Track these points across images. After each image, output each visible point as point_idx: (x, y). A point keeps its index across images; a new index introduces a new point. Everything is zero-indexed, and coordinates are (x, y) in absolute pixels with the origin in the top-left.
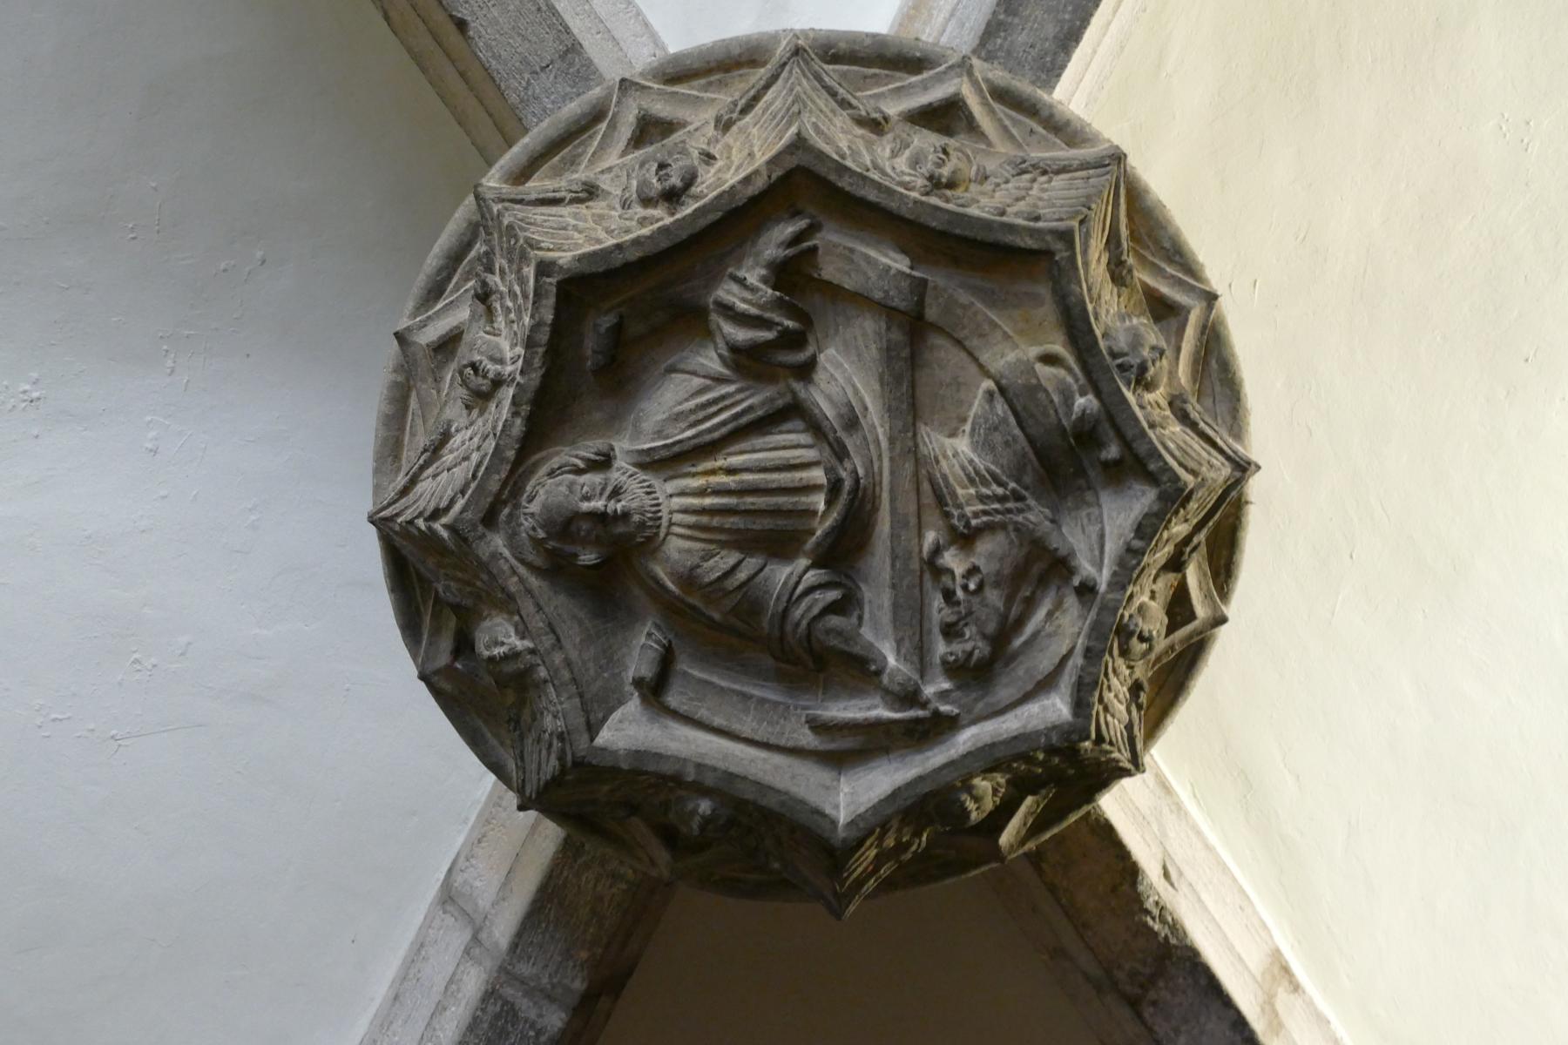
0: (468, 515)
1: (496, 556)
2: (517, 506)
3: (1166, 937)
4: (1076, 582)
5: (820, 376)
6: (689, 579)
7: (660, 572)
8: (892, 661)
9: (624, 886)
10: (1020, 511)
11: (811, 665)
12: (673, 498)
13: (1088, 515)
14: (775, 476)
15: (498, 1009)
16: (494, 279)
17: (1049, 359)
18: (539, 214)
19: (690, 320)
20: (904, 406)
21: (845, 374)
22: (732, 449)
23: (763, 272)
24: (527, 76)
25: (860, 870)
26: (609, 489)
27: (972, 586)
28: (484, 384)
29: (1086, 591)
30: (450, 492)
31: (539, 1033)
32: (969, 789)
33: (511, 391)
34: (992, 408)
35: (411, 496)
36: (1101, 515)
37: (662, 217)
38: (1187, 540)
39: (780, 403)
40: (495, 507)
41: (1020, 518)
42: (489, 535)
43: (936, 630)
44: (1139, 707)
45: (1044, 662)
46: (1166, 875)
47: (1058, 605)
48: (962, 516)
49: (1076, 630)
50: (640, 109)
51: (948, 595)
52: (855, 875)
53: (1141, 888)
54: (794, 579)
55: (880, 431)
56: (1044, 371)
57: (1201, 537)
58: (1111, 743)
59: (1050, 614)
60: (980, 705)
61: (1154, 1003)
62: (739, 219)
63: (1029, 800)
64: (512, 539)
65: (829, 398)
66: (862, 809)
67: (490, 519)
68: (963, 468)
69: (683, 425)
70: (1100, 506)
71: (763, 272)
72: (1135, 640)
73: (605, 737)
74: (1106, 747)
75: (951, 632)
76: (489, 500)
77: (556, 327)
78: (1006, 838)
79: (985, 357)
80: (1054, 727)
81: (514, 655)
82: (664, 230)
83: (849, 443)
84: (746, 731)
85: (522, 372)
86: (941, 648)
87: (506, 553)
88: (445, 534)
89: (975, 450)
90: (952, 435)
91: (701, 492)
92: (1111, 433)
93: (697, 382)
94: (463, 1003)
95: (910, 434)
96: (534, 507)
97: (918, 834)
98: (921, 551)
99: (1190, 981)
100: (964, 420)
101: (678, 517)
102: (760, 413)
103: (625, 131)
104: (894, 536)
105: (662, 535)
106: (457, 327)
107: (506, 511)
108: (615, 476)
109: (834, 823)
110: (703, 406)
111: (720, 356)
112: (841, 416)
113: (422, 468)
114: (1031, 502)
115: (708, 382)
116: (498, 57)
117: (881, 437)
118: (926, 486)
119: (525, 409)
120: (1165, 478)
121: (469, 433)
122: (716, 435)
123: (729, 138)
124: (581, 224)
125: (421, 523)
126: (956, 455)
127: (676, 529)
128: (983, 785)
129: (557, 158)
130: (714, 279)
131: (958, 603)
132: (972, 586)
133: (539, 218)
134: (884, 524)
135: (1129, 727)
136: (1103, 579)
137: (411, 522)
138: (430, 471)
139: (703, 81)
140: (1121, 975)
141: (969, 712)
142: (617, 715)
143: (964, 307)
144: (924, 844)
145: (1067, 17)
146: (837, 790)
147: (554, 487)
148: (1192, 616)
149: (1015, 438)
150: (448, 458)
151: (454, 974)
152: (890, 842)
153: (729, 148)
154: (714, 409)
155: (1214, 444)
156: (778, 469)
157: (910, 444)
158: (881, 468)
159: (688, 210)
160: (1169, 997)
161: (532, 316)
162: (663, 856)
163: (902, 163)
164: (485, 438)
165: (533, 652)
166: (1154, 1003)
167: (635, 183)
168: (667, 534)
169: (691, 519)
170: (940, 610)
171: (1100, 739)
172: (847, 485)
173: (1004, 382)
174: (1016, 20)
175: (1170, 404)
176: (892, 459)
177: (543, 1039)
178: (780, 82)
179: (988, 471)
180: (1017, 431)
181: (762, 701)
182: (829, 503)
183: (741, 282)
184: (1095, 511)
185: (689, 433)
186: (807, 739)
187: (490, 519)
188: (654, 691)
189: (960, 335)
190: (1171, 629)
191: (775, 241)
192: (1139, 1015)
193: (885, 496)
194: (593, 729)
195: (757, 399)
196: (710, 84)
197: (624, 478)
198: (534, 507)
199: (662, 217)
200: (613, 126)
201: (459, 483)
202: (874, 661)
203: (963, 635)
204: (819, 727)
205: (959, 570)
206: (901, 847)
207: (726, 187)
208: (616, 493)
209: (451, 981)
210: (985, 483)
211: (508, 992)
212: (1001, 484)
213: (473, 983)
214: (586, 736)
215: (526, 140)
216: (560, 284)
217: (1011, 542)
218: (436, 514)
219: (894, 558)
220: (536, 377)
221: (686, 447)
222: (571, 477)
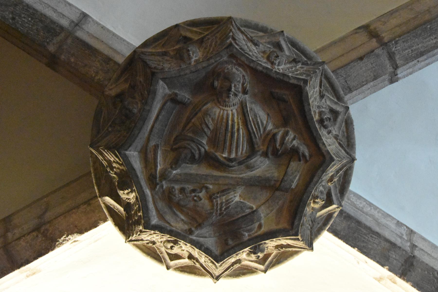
0: (235, 50)
1: (222, 57)
2: (235, 65)
3: (58, 241)
4: (193, 229)
5: (262, 159)
6: (206, 113)
7: (209, 105)
8: (174, 172)
9: (93, 75)
10: (216, 214)
11: (174, 147)
12: (232, 112)
13: (211, 234)
14: (235, 143)
15: (57, 31)
16: (300, 65)
17: (260, 226)
18: (318, 81)
19: (285, 121)
20: (251, 183)
21: (262, 167)
22: (244, 131)
23: (296, 146)
24: (345, 76)
25: (107, 155)
26: (237, 93)
27: (195, 198)
28: (273, 58)
29: (191, 232)
30: (241, 44)
31: (48, 43)
32: (132, 192)
33: (269, 67)
34: (248, 208)
35: (238, 32)
36: (211, 237)
37: (316, 118)
38: (197, 261)
39: (256, 146)
40: (237, 57)
41: (214, 214)
42: (227, 55)
43: (182, 186)
44: (148, 243)
45: (168, 217)
46: (75, 241)
47: (185, 223)
48: (217, 197)
49: (178, 228)
50: (341, 112)
51: (194, 191)
52: (107, 155)
53: (75, 234)
54: (203, 145)
55: (244, 175)
56: (257, 225)
57: (198, 265)
58: (139, 235)
59: (183, 220)
60: (157, 197)
61: (37, 236)
62: (314, 140)
63: (122, 209)
64: (226, 62)
65: (256, 161)
66: (129, 159)
67: (232, 56)
68: (231, 198)
69: (253, 117)
70: (214, 237)
71: (296, 146)
72: (172, 244)
73: (161, 82)
74: (139, 233)
75: (182, 190)
76: (239, 57)
77: (287, 83)
78: (108, 200)
79: (263, 207)
80: (149, 219)
81: (190, 58)
82: (312, 119)
83: (242, 166)
84: (156, 125)
85: (276, 71)
86: (177, 187)
87: (222, 60)
88: (228, 41)
89: (236, 202)
90: (240, 196)
91: (233, 121)
92: (236, 243)
93: (265, 122)
94: (57, 19)
95: (243, 184)
96: (234, 70)
97: (116, 173)
98: (207, 184)
99: (43, 248)
100: (244, 199)
101: (225, 112)
102: (254, 140)
103: (334, 107)
104: (213, 176)
105: (220, 107)
106: (284, 50)
107: (234, 61)
108: (240, 95)
109: (126, 150)
110: (258, 123)
111: (271, 130)
112: (251, 164)
113: (246, 36)
114: (219, 218)
115: (264, 125)
116: (351, 68)
117: (243, 175)
118: (226, 187)
119: (265, 71)
120: (222, 258)
121: (256, 52)
122: (249, 126)
123: (333, 138)
124: (315, 93)
125: (231, 34)
126: (235, 197)
127: (222, 112)
128: (132, 196)
129: (328, 86)
130: (294, 130)
131: (191, 193)
132: (195, 198)
133: (317, 80)
134: (216, 173)
135: (142, 240)
136: (194, 238)
137: (231, 30)
138: (245, 38)
139: (345, 130)
140: (47, 226)
141: (156, 194)
142: (166, 87)
143: (278, 203)
144: (112, 175)
145: (342, 233)
146: (135, 151)
147: (239, 74)
148: (171, 260)
149: (238, 215)
150: (249, 44)
151: (65, 16)
152: (114, 165)
153: (330, 139)
154: (257, 127)
155: (225, 271)
156: (237, 143)
157: (240, 183)
158: (234, 174)
159: (317, 126)
160: (39, 241)
161: (292, 76)
162: (113, 93)
163: (321, 188)
164: (256, 57)
165: (190, 64)
166: (37, 236)
167: (324, 110)
168: (221, 109)
169: (225, 116)
170: (188, 188)
171: (141, 231)
172: (231, 164)
173: (256, 213)
174: (342, 219)
175: (239, 259)
176: (236, 178)
177: (46, 44)
178: (346, 154)
179: (230, 206)
180: (240, 216)
181: (164, 131)
182: (225, 158)
183: (294, 139)
184: (212, 236)
185: (251, 118)
186: (152, 143)
187: (232, 56)
188: (173, 99)
189: (270, 201)
190: (169, 254)
191: (304, 149)
192: (33, 231)
193: (225, 174)
194: (164, 79)
195: (258, 140)
196: (344, 132)
197: (239, 97)
198: (234, 70)
199: (316, 118)
200: (336, 103)
201: (243, 47)
202: (176, 167)
203: (181, 194)
204: (156, 147)
205: (201, 195)
206: (112, 168)
207: (322, 138)
208: (236, 95)
209: (63, 15)
210: (226, 205)
211: (63, 35)
212: (225, 209)
213: (64, 23)
214: (161, 77)
215: (334, 77)
216: (301, 86)
217: (207, 211)
218: (234, 39)
219: (206, 176)
220: (274, 76)
221: (247, 117)
222: (242, 82)
